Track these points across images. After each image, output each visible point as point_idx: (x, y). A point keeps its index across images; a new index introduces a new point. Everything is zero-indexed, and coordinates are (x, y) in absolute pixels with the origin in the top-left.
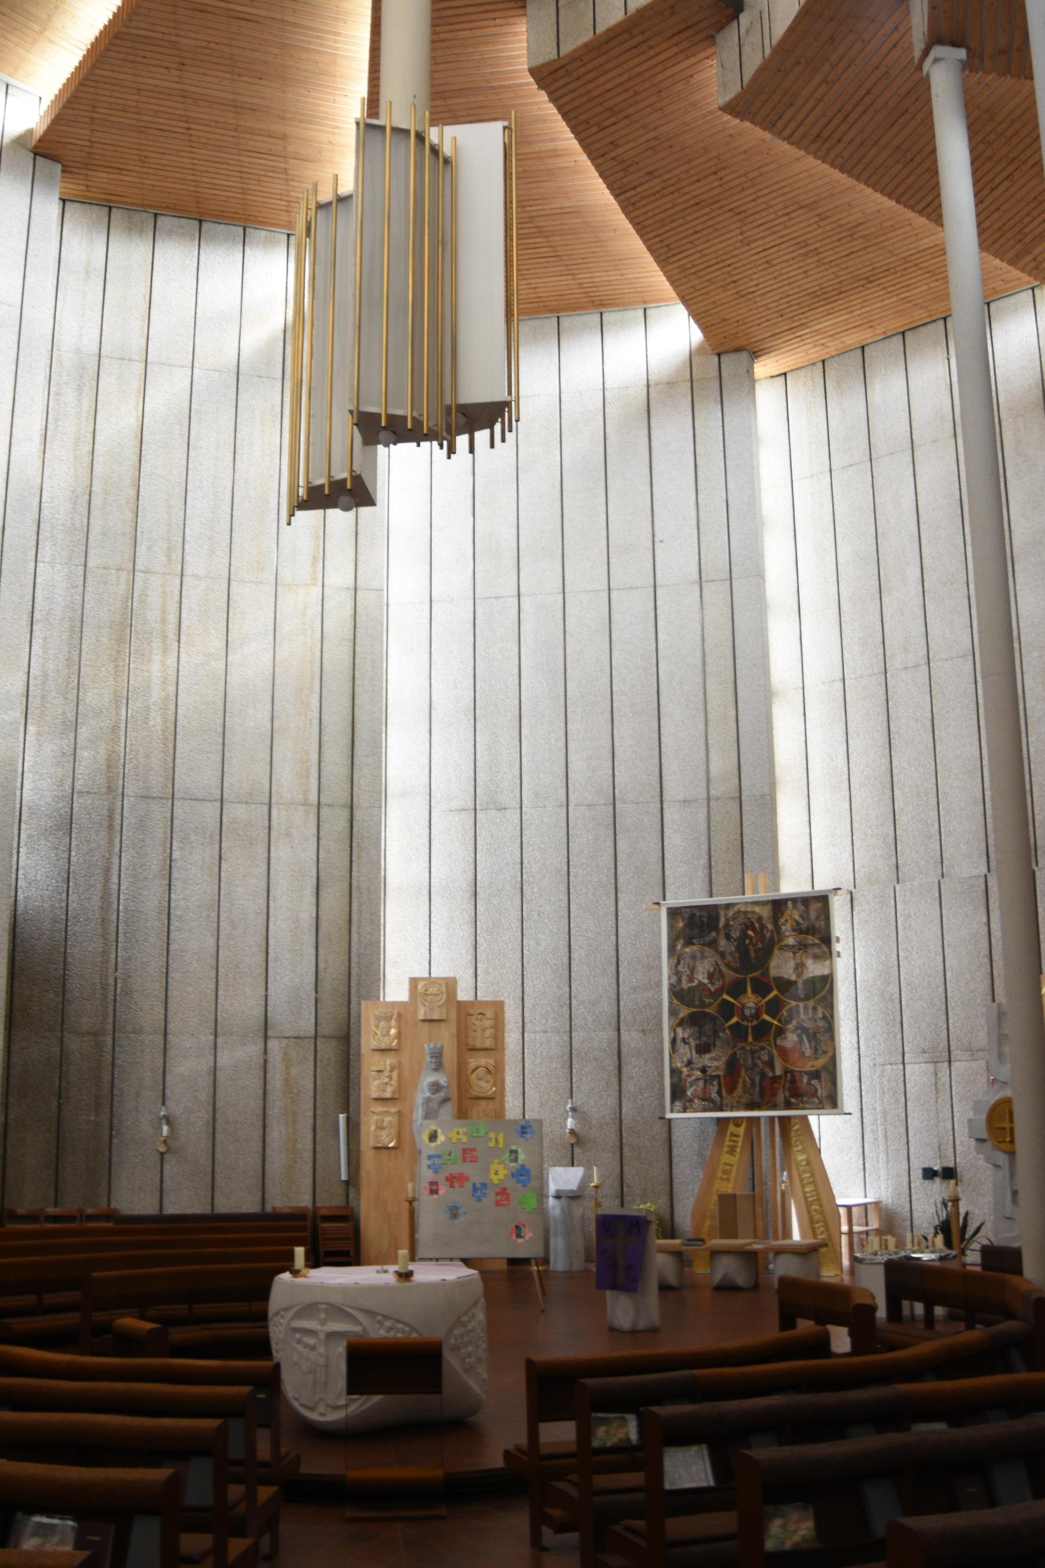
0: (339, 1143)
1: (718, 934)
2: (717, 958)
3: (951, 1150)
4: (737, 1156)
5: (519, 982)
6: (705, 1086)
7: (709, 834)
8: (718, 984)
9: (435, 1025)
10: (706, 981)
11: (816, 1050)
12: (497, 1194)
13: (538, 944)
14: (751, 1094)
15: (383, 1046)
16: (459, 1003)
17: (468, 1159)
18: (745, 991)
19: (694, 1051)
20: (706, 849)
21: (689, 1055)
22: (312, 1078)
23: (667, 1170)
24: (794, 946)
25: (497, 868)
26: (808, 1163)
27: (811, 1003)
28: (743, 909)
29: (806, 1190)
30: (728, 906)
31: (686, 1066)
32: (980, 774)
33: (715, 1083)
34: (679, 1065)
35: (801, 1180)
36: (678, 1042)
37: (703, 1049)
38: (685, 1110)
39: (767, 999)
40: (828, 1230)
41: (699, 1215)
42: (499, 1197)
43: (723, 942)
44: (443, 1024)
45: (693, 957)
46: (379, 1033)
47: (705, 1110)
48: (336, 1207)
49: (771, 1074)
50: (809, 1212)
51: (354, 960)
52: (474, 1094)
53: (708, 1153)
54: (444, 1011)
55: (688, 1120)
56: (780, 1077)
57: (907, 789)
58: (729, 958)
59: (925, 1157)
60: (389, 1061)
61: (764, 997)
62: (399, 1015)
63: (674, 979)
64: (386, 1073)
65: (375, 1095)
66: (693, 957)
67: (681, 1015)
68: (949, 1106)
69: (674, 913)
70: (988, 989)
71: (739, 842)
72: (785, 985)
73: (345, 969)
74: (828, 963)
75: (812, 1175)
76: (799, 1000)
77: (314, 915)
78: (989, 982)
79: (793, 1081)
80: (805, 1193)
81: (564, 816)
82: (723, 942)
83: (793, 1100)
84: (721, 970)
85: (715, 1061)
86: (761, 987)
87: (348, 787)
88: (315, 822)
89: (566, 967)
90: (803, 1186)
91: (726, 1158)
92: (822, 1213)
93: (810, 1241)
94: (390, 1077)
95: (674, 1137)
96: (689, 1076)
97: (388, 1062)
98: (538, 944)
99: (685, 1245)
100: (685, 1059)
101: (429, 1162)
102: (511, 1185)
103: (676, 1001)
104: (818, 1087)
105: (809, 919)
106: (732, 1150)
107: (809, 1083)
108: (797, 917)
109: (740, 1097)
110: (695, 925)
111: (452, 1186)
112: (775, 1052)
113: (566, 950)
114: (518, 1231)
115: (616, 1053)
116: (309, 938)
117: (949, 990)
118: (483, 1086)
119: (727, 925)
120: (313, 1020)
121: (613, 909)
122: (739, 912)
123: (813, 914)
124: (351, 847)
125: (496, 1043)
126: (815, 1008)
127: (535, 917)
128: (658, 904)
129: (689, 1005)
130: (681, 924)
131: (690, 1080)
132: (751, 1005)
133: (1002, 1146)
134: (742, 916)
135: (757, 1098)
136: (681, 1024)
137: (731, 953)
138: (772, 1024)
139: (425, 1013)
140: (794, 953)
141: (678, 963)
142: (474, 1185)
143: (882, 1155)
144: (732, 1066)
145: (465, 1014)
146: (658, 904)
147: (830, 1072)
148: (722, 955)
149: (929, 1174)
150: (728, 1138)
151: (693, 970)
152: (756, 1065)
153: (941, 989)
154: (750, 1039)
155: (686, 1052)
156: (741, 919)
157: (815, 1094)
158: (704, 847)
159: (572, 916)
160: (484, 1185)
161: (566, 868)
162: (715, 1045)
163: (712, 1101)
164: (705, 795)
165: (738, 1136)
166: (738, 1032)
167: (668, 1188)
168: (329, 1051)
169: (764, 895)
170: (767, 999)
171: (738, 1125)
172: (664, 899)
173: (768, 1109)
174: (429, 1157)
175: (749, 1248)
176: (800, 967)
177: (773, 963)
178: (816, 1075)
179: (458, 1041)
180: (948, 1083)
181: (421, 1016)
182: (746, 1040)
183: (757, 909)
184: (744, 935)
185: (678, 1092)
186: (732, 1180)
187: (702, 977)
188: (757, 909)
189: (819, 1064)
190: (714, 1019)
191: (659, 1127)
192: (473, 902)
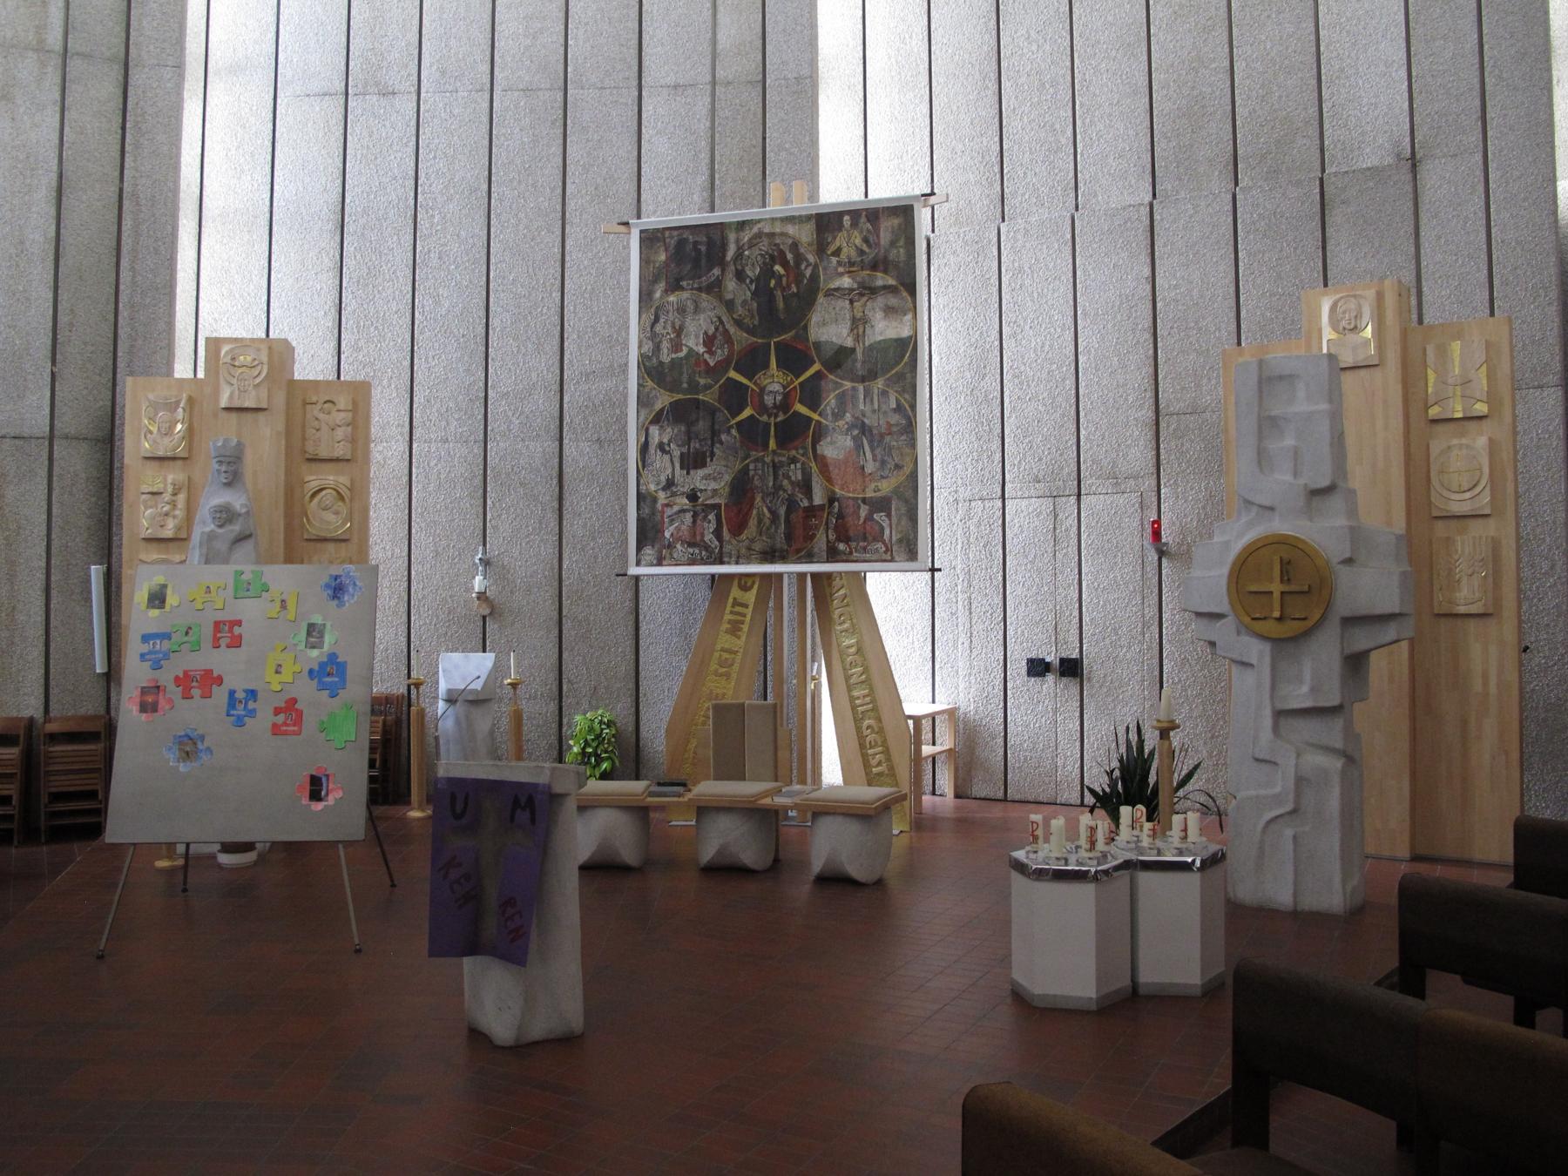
0: (91, 613)
1: (723, 271)
2: (722, 311)
3: (1075, 631)
4: (743, 638)
5: (407, 363)
6: (694, 522)
7: (713, 137)
8: (721, 354)
9: (249, 416)
10: (701, 349)
11: (883, 463)
12: (277, 711)
13: (437, 303)
14: (771, 537)
15: (161, 453)
16: (292, 384)
17: (223, 642)
18: (766, 366)
19: (677, 466)
20: (707, 161)
21: (669, 471)
22: (44, 504)
23: (631, 657)
24: (852, 290)
25: (378, 183)
26: (859, 651)
27: (880, 383)
28: (767, 230)
29: (855, 694)
30: (742, 225)
31: (664, 489)
32: (1145, 49)
33: (711, 517)
34: (652, 487)
35: (847, 678)
36: (652, 449)
37: (692, 461)
38: (659, 564)
39: (802, 379)
40: (889, 759)
41: (679, 730)
42: (281, 718)
43: (731, 285)
44: (261, 416)
45: (681, 310)
46: (154, 429)
47: (692, 562)
48: (86, 718)
49: (805, 503)
50: (859, 730)
51: (124, 313)
52: (314, 532)
53: (695, 632)
54: (264, 393)
55: (670, 579)
56: (821, 507)
57: (1023, 79)
58: (740, 310)
59: (1030, 641)
60: (174, 475)
61: (797, 377)
62: (191, 400)
63: (648, 347)
64: (167, 497)
65: (149, 533)
66: (681, 310)
67: (658, 406)
68: (1074, 564)
69: (650, 239)
70: (1148, 383)
71: (759, 150)
72: (838, 359)
73: (107, 330)
74: (909, 316)
75: (866, 671)
76: (863, 380)
77: (53, 234)
78: (1151, 370)
79: (841, 516)
80: (852, 699)
81: (486, 105)
82: (731, 285)
83: (842, 546)
84: (726, 331)
85: (712, 481)
86: (794, 359)
87: (119, 30)
88: (58, 80)
89: (481, 340)
90: (849, 689)
91: (725, 641)
92: (881, 731)
93: (868, 793)
94: (174, 505)
95: (643, 607)
96: (667, 505)
97: (170, 478)
98: (437, 303)
99: (652, 794)
100: (663, 478)
101: (145, 648)
102: (306, 693)
103: (650, 383)
104: (885, 525)
105: (878, 244)
106: (735, 629)
107: (869, 518)
108: (858, 241)
109: (752, 541)
110: (686, 258)
111: (187, 696)
112: (813, 465)
113: (482, 313)
114: (316, 789)
115: (555, 473)
116: (41, 273)
117: (1082, 384)
118: (328, 519)
119: (739, 255)
120: (47, 410)
121: (557, 250)
122: (760, 235)
123: (885, 237)
124: (123, 128)
125: (354, 450)
126: (884, 393)
127: (435, 262)
128: (626, 224)
129: (673, 387)
130: (663, 257)
131: (669, 512)
132: (777, 387)
133: (1259, 626)
134: (766, 241)
135: (780, 541)
136: (657, 420)
137: (745, 302)
138: (809, 419)
139: (231, 397)
140: (851, 302)
141: (656, 320)
142: (232, 693)
143: (963, 638)
144: (741, 489)
145: (300, 399)
146: (626, 224)
147: (905, 500)
148: (730, 305)
149: (1037, 668)
150: (729, 608)
151: (679, 331)
152: (781, 487)
153: (1070, 382)
154: (772, 444)
155: (663, 466)
156: (764, 246)
157: (879, 537)
158: (704, 156)
159: (493, 260)
160: (252, 694)
161: (485, 186)
162: (712, 455)
163: (707, 548)
164: (708, 78)
165: (746, 606)
166: (752, 434)
167: (632, 685)
168: (75, 462)
169: (800, 206)
170: (802, 379)
171: (745, 588)
172: (639, 217)
173: (799, 561)
174: (146, 638)
175: (767, 801)
176: (859, 324)
177: (815, 318)
178: (882, 505)
179: (289, 447)
180: (1075, 529)
181: (224, 403)
182: (766, 446)
183: (791, 230)
184: (767, 272)
185: (648, 533)
186: (734, 676)
187: (693, 342)
188: (791, 230)
189: (886, 487)
190: (712, 412)
191: (620, 594)
192: (338, 238)
